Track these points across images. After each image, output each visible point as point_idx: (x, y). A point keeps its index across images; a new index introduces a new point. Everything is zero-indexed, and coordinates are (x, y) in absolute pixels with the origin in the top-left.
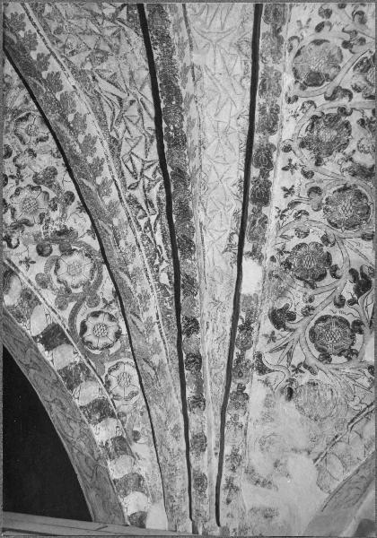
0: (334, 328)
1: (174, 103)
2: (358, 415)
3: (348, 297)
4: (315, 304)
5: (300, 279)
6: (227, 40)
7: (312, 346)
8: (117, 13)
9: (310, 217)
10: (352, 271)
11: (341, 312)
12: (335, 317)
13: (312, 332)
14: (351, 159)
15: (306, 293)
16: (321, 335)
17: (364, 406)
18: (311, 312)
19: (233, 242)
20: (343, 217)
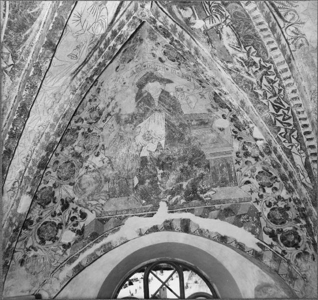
0: (49, 227)
1: (22, 117)
2: (56, 269)
3: (58, 212)
4: (43, 215)
5: (39, 204)
6: (52, 91)
7: (37, 237)
8: (6, 67)
9: (52, 175)
10: (62, 200)
11: (53, 219)
12: (50, 222)
13: (39, 230)
14: (74, 149)
15: (40, 211)
16: (43, 231)
17: (59, 264)
18: (41, 220)
19: (15, 186)
20: (64, 175)
